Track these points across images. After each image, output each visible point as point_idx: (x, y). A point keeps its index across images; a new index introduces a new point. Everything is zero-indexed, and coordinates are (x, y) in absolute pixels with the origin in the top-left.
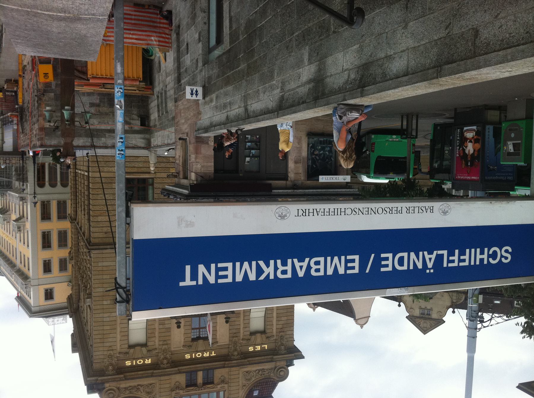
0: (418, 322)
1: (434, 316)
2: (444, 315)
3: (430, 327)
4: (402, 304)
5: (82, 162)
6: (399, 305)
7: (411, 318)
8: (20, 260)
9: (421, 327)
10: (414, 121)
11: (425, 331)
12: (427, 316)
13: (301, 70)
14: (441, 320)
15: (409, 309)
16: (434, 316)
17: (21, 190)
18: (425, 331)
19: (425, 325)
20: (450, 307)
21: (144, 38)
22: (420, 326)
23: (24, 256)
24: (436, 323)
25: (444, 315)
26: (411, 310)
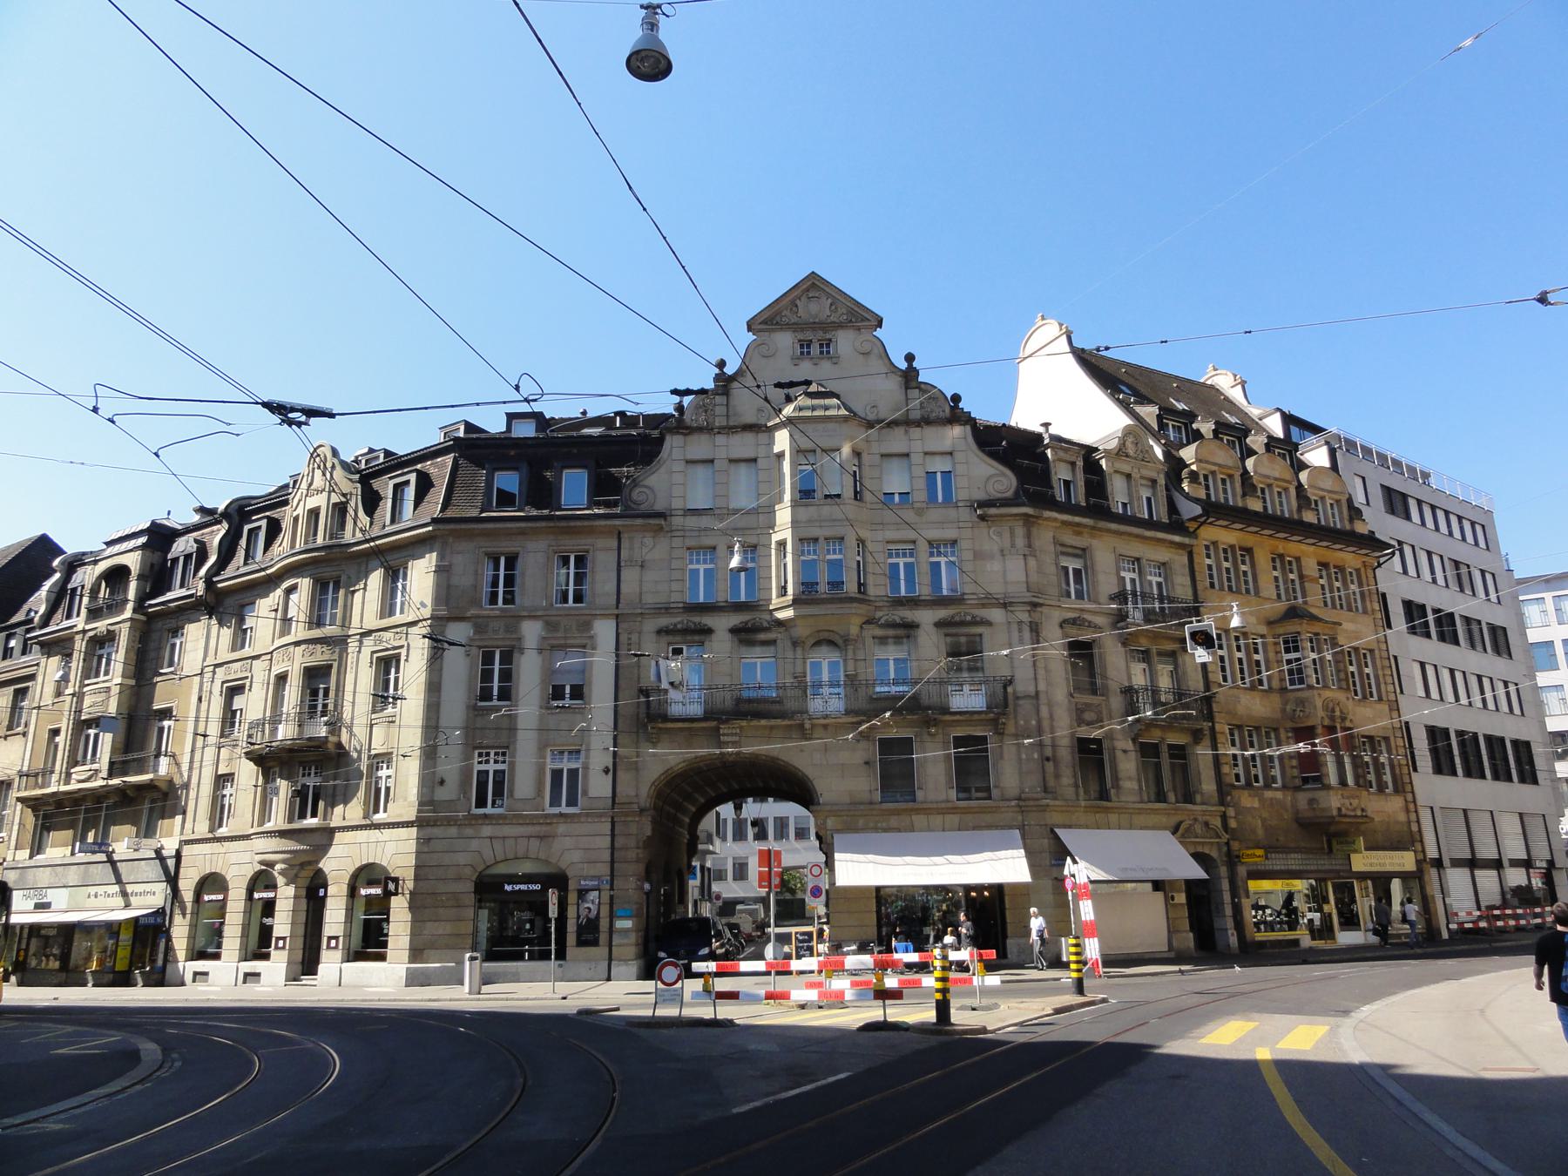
0: (840, 311)
1: (785, 341)
2: (751, 350)
3: (798, 302)
4: (903, 365)
5: (887, 1011)
6: (910, 358)
7: (864, 319)
8: (1408, 562)
9: (829, 295)
10: (268, 714)
11: (813, 285)
12: (809, 335)
13: (164, 762)
14: (760, 331)
15: (876, 351)
16: (785, 341)
17: (635, 806)
18: (813, 285)
19: (814, 307)
20: (732, 378)
21: (238, 931)
22: (830, 301)
23: (1462, 590)
24: (778, 318)
25: (751, 350)
26: (867, 347)
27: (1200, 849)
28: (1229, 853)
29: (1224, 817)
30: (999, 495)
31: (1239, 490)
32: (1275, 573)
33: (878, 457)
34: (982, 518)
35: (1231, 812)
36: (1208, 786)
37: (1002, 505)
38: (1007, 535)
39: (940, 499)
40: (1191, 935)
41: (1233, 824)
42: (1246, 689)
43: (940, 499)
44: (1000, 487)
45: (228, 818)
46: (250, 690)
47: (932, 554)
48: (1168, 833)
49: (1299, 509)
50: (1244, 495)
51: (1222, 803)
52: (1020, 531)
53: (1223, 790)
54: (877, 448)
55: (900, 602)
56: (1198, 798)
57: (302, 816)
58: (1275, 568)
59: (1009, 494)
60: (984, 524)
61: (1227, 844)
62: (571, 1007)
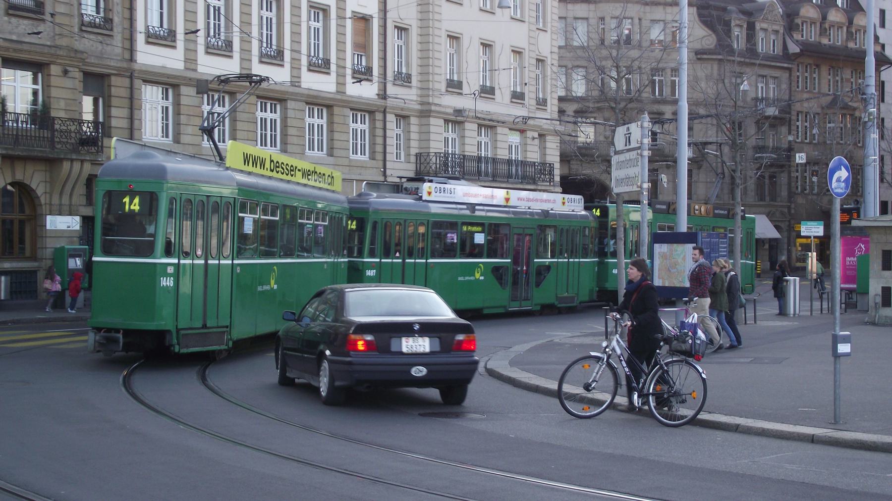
27: (777, 224)
28: (789, 226)
29: (789, 208)
30: (708, 47)
31: (818, 32)
32: (829, 77)
33: (649, 21)
34: (699, 59)
35: (793, 206)
36: (784, 193)
37: (710, 54)
38: (709, 68)
39: (716, 212)
40: (769, 263)
41: (793, 211)
42: (807, 143)
43: (716, 212)
44: (708, 42)
45: (440, 105)
46: (220, 389)
47: (672, 76)
48: (764, 216)
49: (847, 40)
50: (821, 35)
51: (790, 202)
52: (716, 67)
53: (791, 195)
54: (650, 17)
55: (657, 102)
56: (779, 199)
57: (317, 390)
58: (830, 75)
59: (712, 47)
60: (699, 62)
61: (789, 221)
62: (537, 207)
